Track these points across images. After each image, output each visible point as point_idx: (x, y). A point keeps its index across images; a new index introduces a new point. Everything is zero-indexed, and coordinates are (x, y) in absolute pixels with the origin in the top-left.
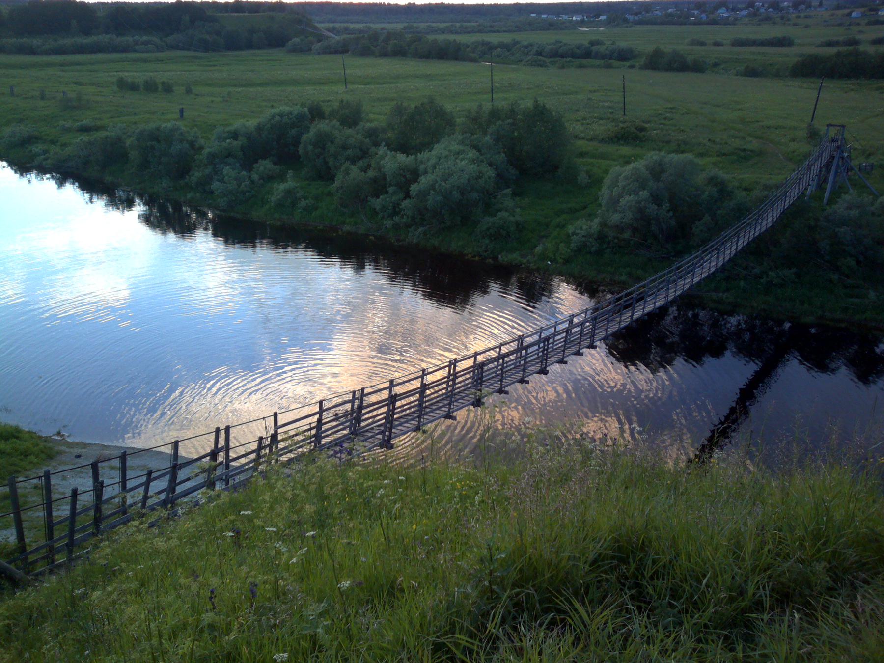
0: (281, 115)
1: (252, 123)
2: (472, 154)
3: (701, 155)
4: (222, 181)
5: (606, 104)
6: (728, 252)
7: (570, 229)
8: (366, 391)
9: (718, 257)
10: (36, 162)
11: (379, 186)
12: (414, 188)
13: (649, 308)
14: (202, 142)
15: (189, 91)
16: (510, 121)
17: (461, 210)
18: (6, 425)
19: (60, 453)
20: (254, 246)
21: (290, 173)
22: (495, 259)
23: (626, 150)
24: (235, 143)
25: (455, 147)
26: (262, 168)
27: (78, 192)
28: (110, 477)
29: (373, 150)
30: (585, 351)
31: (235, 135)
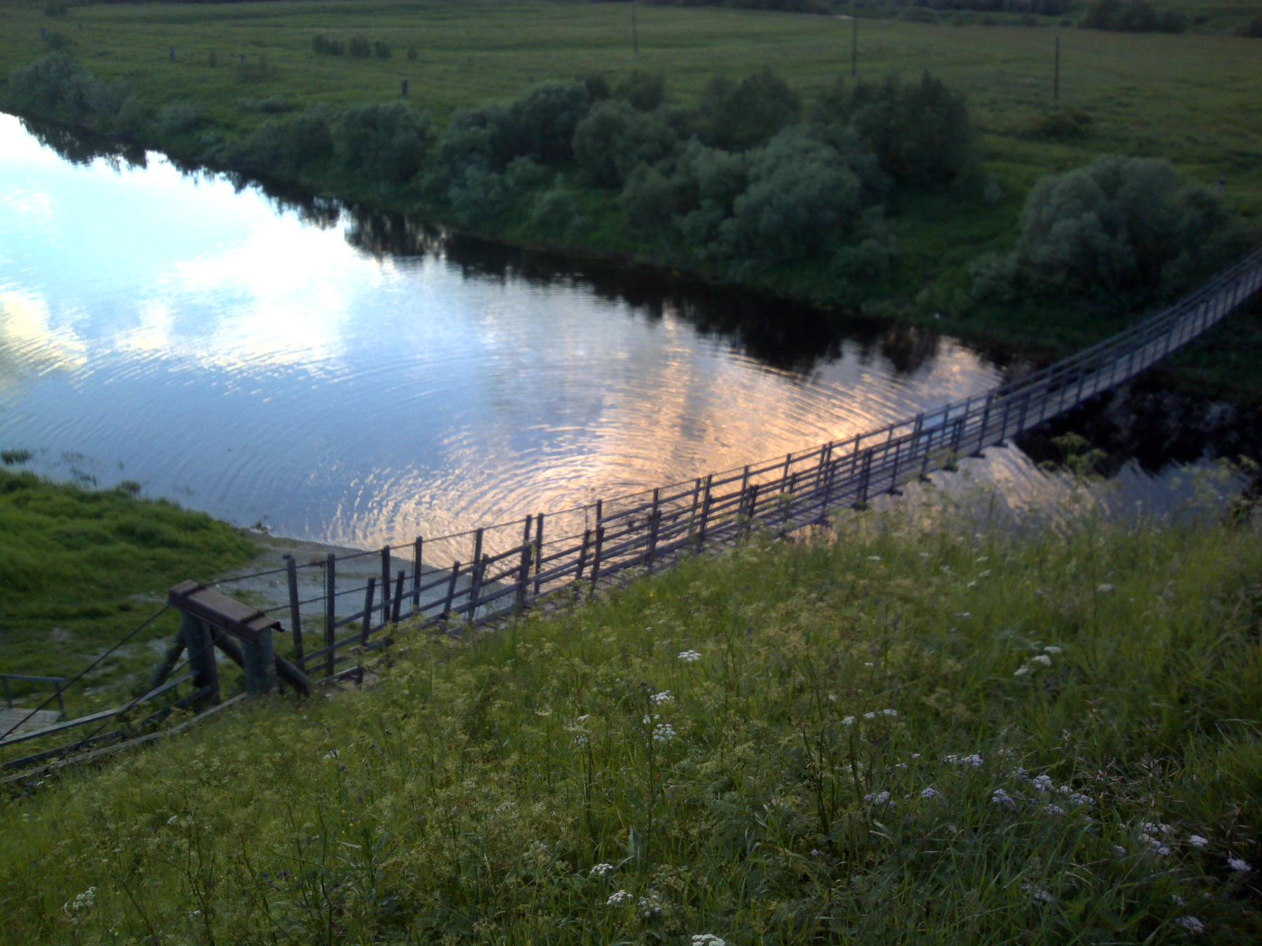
0: (548, 92)
1: (505, 103)
2: (827, 152)
3: (1176, 161)
4: (463, 186)
5: (1027, 81)
6: (1221, 306)
7: (972, 267)
8: (714, 480)
9: (1206, 314)
10: (208, 152)
11: (688, 198)
12: (741, 202)
13: (1087, 392)
14: (434, 130)
15: (412, 56)
16: (884, 104)
17: (809, 234)
18: (189, 511)
19: (263, 551)
20: (503, 284)
21: (560, 177)
22: (857, 308)
23: (1058, 151)
24: (482, 132)
25: (802, 142)
26: (519, 169)
27: (263, 197)
28: (311, 590)
29: (679, 145)
30: (989, 452)
31: (482, 121)
